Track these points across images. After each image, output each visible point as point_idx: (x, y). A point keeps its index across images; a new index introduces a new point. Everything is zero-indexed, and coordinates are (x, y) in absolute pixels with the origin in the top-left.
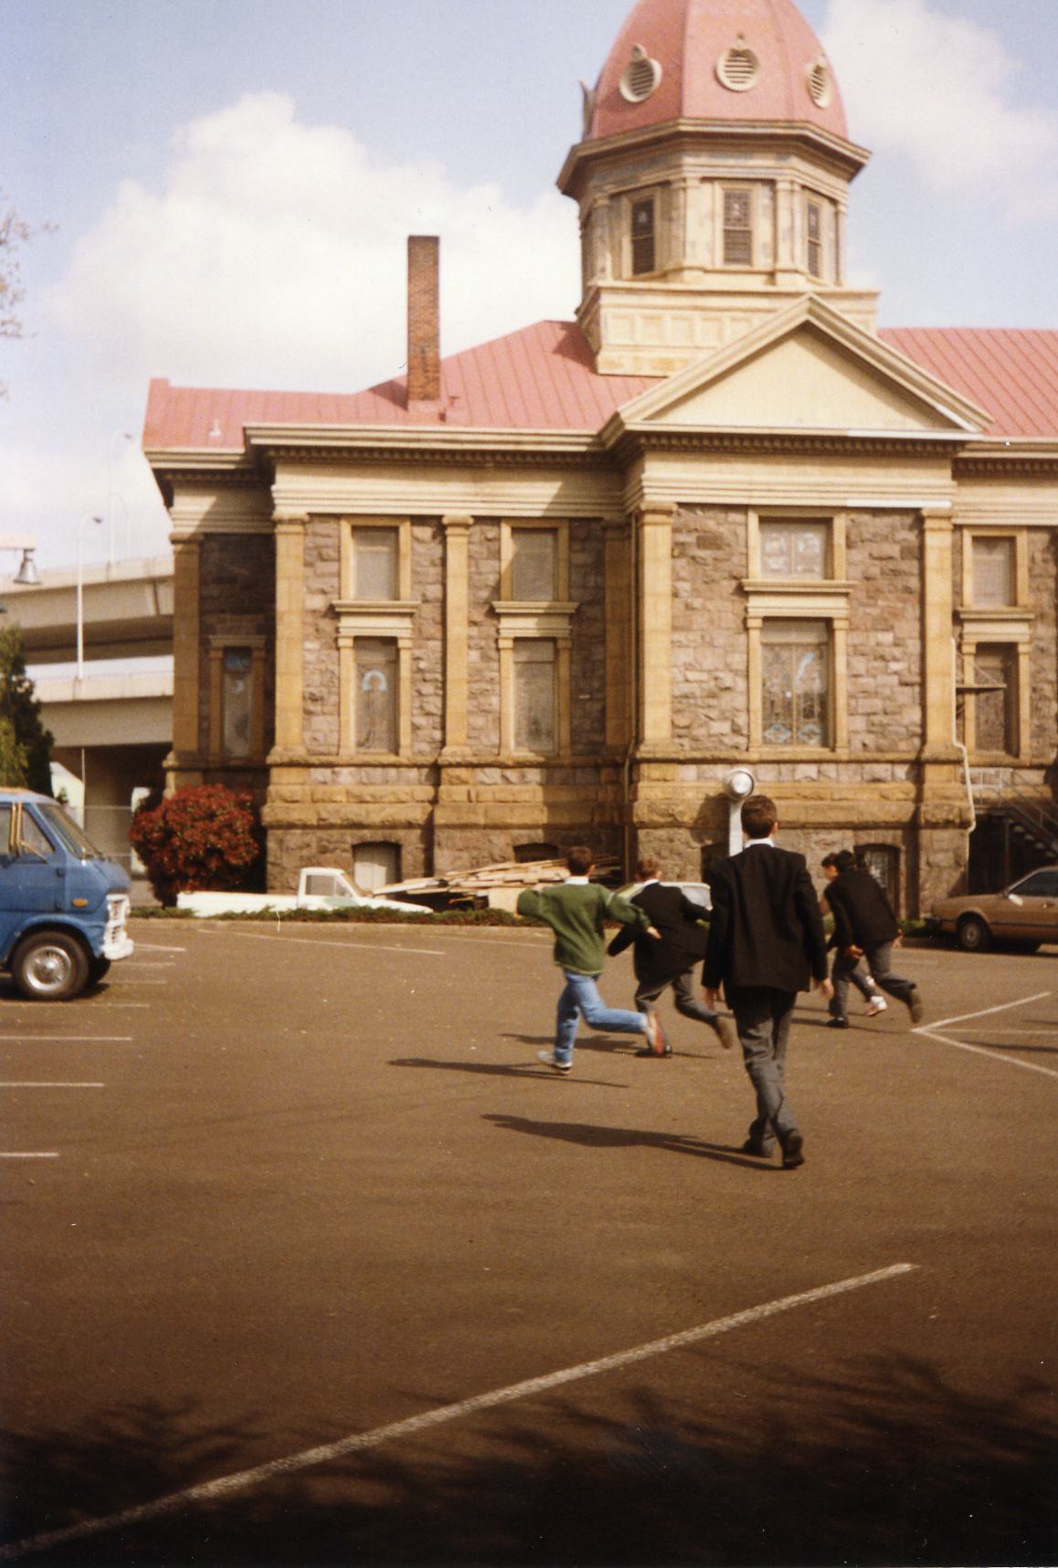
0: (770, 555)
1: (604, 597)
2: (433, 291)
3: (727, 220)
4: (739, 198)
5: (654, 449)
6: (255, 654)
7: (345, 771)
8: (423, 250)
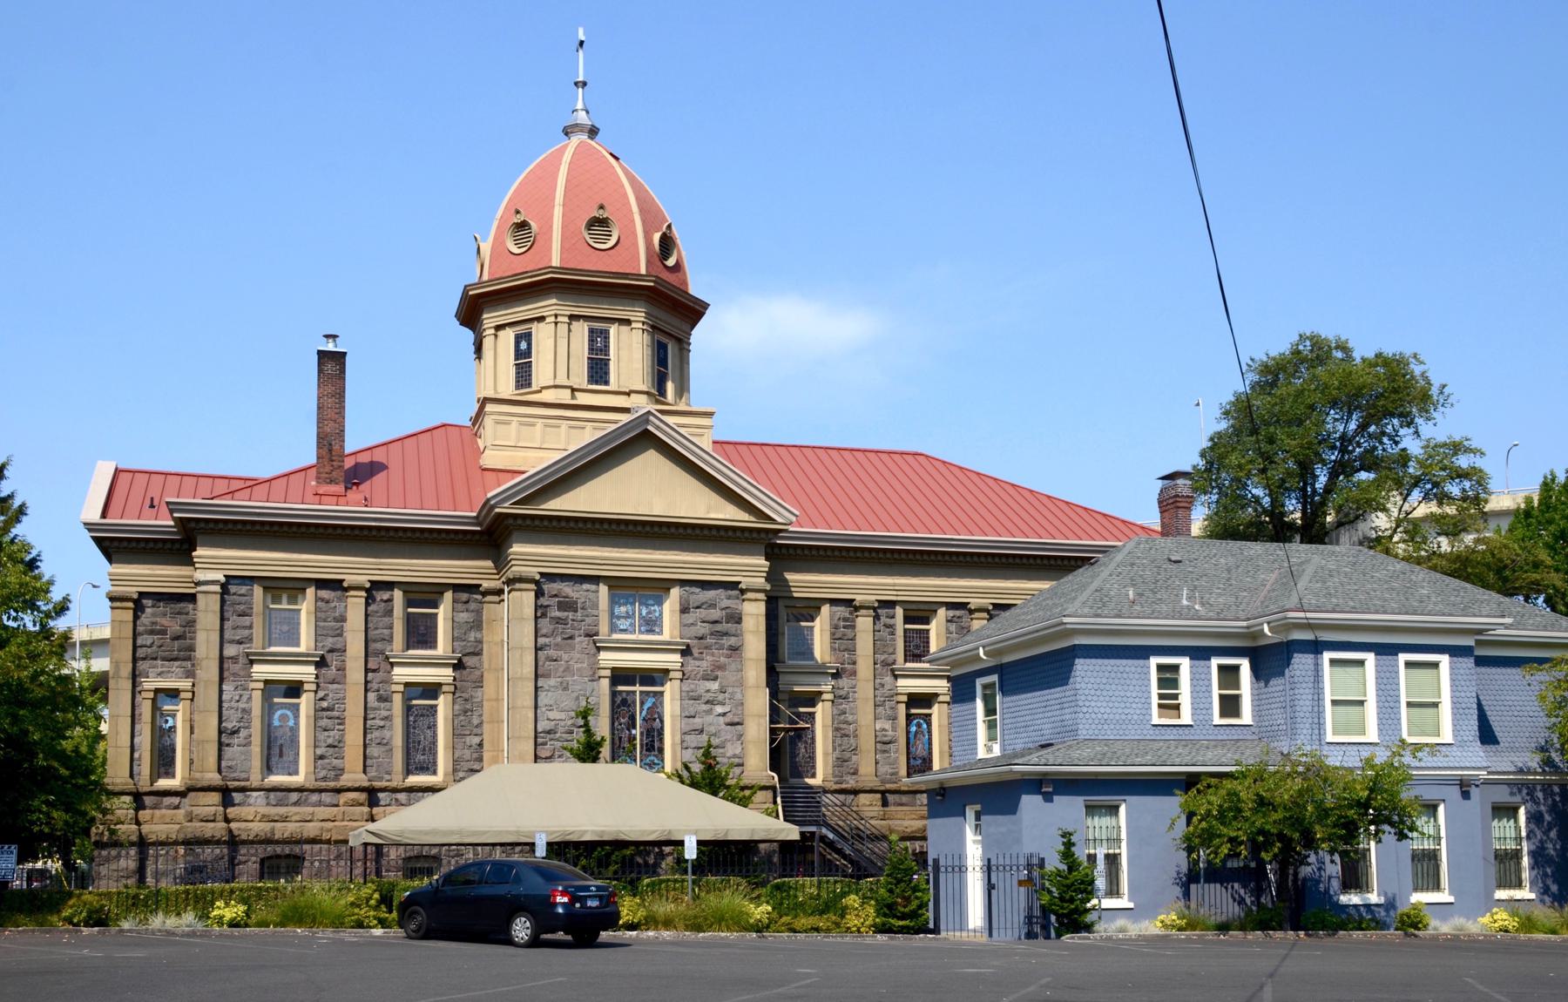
0: (619, 618)
1: (482, 650)
2: (340, 395)
3: (591, 350)
4: (601, 333)
5: (520, 528)
6: (183, 695)
7: (255, 794)
8: (332, 364)
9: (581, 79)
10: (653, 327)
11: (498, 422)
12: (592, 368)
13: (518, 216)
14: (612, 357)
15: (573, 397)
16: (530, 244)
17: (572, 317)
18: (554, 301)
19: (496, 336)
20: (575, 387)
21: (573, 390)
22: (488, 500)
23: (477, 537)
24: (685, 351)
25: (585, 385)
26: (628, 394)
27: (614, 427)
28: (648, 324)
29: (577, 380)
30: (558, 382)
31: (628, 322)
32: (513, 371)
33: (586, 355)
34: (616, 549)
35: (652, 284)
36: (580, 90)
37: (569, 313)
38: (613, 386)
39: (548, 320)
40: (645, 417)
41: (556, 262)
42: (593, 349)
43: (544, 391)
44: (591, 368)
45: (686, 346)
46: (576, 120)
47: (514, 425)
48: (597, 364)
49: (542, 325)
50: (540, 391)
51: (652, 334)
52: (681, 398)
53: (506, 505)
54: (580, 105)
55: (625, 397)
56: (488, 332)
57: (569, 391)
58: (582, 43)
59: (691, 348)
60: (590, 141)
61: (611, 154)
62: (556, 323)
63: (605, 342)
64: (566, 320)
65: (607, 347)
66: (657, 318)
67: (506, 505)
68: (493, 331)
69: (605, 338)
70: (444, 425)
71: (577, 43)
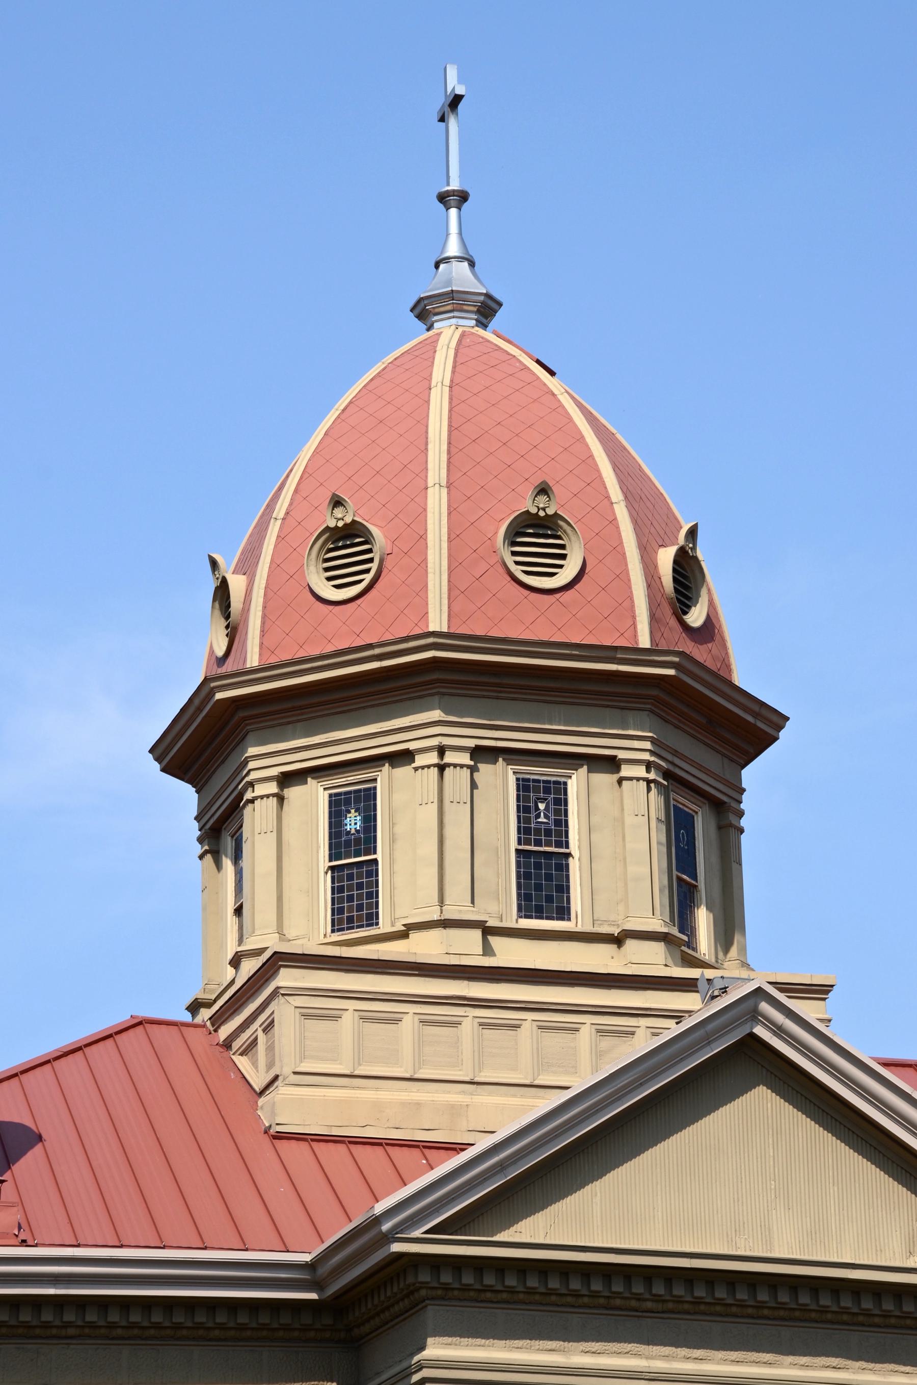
3: (524, 832)
4: (547, 791)
5: (445, 1294)
9: (454, 185)
10: (667, 775)
11: (308, 1015)
12: (527, 876)
13: (339, 512)
14: (574, 848)
15: (488, 950)
16: (368, 577)
17: (481, 754)
18: (436, 715)
19: (281, 799)
20: (492, 923)
21: (488, 931)
22: (377, 1220)
23: (306, 1319)
24: (732, 831)
25: (512, 920)
26: (618, 940)
27: (673, 1029)
28: (658, 767)
29: (493, 907)
30: (451, 913)
31: (611, 764)
32: (325, 884)
33: (513, 845)
34: (683, 1352)
35: (671, 672)
36: (453, 212)
37: (472, 743)
38: (578, 922)
39: (420, 760)
40: (750, 1003)
41: (437, 621)
42: (527, 831)
43: (413, 935)
44: (523, 877)
45: (732, 818)
46: (449, 282)
47: (348, 1020)
48: (538, 866)
49: (403, 772)
50: (403, 935)
51: (664, 791)
52: (726, 951)
53: (417, 1233)
54: (453, 248)
55: (610, 948)
56: (261, 790)
57: (477, 934)
58: (456, 101)
59: (743, 822)
60: (480, 331)
61: (538, 362)
62: (442, 768)
63: (557, 812)
64: (465, 759)
65: (562, 824)
66: (675, 753)
67: (417, 1233)
68: (273, 788)
69: (557, 802)
70: (139, 1023)
71: (440, 102)
